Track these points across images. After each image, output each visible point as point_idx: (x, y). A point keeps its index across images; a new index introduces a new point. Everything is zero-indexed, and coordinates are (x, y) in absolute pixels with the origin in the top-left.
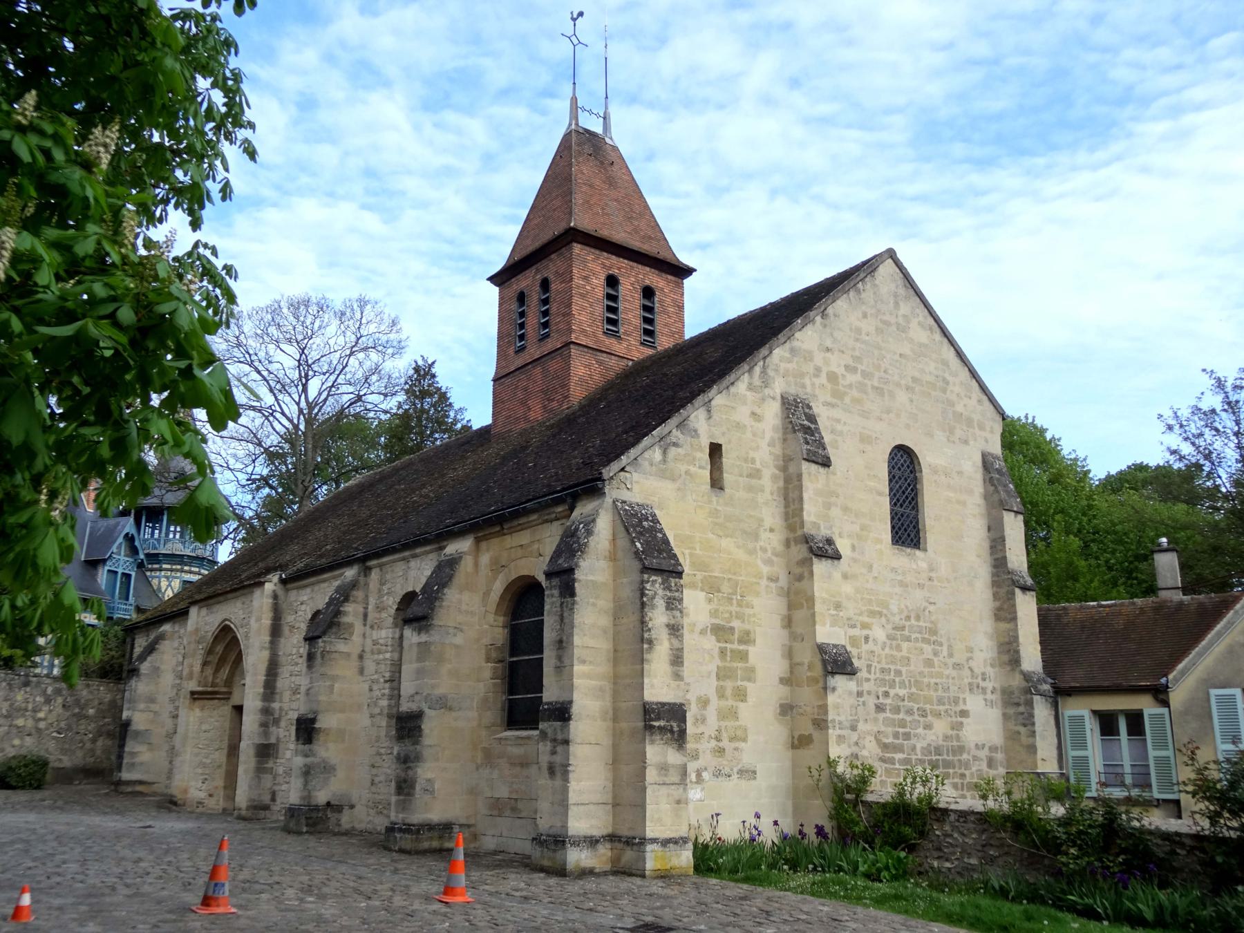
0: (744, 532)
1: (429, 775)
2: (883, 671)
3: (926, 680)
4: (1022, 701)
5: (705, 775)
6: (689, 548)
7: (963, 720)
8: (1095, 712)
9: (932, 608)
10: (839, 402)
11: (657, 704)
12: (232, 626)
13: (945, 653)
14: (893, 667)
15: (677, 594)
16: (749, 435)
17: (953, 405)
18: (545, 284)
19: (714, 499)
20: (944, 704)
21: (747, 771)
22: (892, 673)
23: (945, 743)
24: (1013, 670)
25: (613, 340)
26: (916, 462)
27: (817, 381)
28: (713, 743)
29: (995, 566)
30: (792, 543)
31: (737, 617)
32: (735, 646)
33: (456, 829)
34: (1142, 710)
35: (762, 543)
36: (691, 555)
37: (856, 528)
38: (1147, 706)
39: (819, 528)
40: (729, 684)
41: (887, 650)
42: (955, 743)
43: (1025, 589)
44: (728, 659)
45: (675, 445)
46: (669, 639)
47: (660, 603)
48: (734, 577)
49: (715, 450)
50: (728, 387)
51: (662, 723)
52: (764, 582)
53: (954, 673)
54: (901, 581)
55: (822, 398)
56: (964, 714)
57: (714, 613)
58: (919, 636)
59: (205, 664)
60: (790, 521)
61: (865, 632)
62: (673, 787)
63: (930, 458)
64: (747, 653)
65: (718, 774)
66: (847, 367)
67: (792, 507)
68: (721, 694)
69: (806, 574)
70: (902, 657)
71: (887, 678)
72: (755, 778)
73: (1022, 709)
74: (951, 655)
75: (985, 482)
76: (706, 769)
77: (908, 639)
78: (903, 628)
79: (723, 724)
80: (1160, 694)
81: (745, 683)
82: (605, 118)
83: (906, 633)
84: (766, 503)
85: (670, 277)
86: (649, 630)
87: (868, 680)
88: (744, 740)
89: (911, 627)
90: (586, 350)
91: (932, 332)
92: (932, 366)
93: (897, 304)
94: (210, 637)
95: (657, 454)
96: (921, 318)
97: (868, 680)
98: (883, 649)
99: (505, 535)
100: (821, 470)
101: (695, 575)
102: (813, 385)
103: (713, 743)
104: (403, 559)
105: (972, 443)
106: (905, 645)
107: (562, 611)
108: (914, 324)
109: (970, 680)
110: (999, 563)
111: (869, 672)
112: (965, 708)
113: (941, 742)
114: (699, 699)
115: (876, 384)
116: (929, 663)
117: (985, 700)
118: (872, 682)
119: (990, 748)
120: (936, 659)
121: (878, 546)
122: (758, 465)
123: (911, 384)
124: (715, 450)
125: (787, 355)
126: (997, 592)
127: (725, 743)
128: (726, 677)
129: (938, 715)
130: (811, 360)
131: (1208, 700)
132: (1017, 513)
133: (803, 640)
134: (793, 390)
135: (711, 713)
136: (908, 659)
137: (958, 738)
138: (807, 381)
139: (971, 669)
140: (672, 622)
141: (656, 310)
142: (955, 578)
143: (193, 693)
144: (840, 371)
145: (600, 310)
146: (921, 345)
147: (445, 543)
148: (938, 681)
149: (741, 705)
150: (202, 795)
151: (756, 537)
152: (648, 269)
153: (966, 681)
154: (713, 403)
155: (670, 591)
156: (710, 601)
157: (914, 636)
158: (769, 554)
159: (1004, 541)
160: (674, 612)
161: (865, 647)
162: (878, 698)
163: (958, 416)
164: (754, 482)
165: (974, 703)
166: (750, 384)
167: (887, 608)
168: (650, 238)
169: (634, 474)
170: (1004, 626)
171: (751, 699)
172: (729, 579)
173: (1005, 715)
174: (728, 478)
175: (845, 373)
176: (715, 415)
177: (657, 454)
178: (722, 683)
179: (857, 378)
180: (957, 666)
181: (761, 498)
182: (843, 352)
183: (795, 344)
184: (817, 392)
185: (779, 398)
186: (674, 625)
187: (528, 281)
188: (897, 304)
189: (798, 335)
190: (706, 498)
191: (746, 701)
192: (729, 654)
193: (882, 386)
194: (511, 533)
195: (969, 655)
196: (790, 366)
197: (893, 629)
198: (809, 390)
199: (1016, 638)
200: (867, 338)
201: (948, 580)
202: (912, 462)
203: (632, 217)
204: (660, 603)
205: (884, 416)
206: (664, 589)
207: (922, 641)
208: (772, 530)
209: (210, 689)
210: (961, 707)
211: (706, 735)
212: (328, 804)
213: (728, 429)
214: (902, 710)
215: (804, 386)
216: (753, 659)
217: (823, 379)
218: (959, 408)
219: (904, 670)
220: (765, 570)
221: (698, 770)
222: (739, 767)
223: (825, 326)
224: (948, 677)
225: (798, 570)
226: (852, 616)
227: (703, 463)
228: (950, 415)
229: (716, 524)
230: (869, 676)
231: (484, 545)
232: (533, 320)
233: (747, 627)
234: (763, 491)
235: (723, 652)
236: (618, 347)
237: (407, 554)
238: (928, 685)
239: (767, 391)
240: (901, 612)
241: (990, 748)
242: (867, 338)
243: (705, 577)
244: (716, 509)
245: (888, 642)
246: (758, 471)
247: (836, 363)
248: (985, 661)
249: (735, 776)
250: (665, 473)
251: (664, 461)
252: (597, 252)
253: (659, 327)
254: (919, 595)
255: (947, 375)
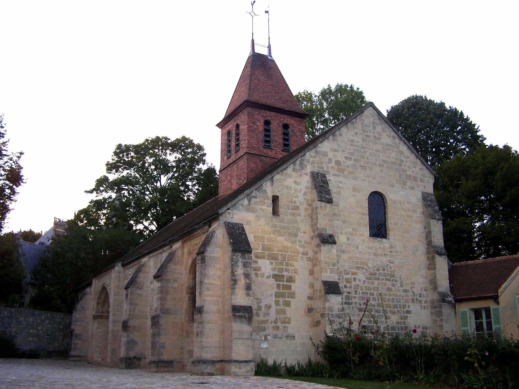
0: (290, 234)
1: (163, 341)
2: (363, 293)
3: (387, 297)
4: (437, 306)
5: (269, 337)
6: (261, 241)
7: (407, 315)
8: (472, 309)
9: (391, 265)
10: (341, 174)
11: (238, 306)
12: (106, 286)
13: (399, 285)
14: (369, 292)
15: (248, 261)
16: (293, 191)
17: (406, 171)
18: (238, 126)
19: (275, 220)
20: (397, 308)
21: (291, 336)
22: (369, 294)
23: (397, 325)
24: (434, 292)
25: (268, 151)
26: (385, 199)
27: (330, 165)
28: (273, 324)
29: (428, 245)
30: (314, 238)
31: (286, 271)
32: (285, 283)
33: (175, 363)
34: (490, 307)
35: (299, 238)
36: (262, 245)
37: (350, 230)
38: (492, 305)
39: (326, 230)
40: (281, 300)
41: (366, 284)
42: (403, 325)
43: (440, 254)
44: (281, 289)
45: (255, 197)
46: (245, 279)
47: (240, 264)
48: (284, 253)
49: (275, 199)
50: (282, 171)
51: (240, 314)
52: (300, 255)
53: (404, 294)
54: (375, 253)
55: (332, 172)
56: (408, 312)
57: (273, 269)
58: (384, 277)
59: (98, 303)
60: (314, 228)
61: (353, 276)
62: (245, 340)
63: (390, 196)
64: (291, 286)
65: (275, 337)
66: (346, 158)
67: (314, 222)
68: (277, 303)
69: (319, 251)
70: (374, 287)
71: (366, 296)
72: (294, 339)
73: (438, 309)
74: (402, 286)
75: (423, 206)
76: (269, 335)
77: (378, 279)
78: (375, 274)
79: (278, 316)
80: (496, 299)
81: (290, 299)
82: (269, 47)
83: (377, 276)
84: (302, 221)
85: (297, 119)
86: (235, 276)
87: (355, 297)
88: (289, 323)
89: (380, 274)
90: (254, 155)
91: (394, 139)
92: (394, 155)
93: (374, 128)
94: (99, 292)
95: (246, 202)
96: (388, 133)
97: (355, 297)
98: (364, 284)
99: (191, 240)
100: (328, 205)
101: (264, 253)
102: (328, 167)
103: (273, 324)
104: (161, 253)
105: (416, 188)
106: (376, 282)
107: (201, 269)
108: (384, 135)
109: (413, 297)
110: (429, 243)
111: (356, 294)
112: (409, 310)
113: (395, 325)
114: (266, 305)
115: (362, 164)
116: (389, 289)
117: (421, 306)
118: (357, 298)
119: (423, 328)
120: (393, 288)
121: (362, 238)
122: (298, 204)
123: (381, 163)
124: (275, 199)
125: (314, 154)
126: (428, 257)
127: (279, 324)
128: (279, 296)
129: (394, 313)
130: (327, 156)
131: (515, 300)
132: (438, 220)
133: (317, 280)
134: (316, 170)
135: (273, 311)
136: (378, 288)
137: (404, 323)
138: (324, 165)
139: (413, 292)
140: (246, 272)
141: (290, 134)
142: (405, 251)
143: (94, 316)
144: (342, 160)
145: (261, 137)
146: (387, 145)
147: (173, 245)
148: (394, 297)
149: (287, 308)
150: (100, 359)
151: (296, 235)
152: (286, 116)
153: (410, 297)
154: (274, 178)
155: (245, 259)
156: (272, 263)
157: (381, 278)
158: (303, 243)
159: (431, 233)
160: (247, 268)
161: (354, 283)
162: (360, 305)
163: (409, 177)
164: (295, 212)
165: (414, 308)
166: (294, 168)
167: (367, 265)
168: (288, 101)
169: (234, 211)
170: (430, 272)
171: (293, 306)
172: (282, 255)
173: (432, 313)
174: (281, 210)
175: (345, 161)
176: (276, 184)
177: (246, 202)
178: (277, 299)
179: (352, 162)
180: (405, 291)
181: (299, 219)
182: (344, 151)
183: (318, 149)
184: (330, 170)
185: (309, 173)
186: (247, 274)
187: (231, 126)
188: (374, 128)
189: (319, 145)
190: (270, 219)
191: (290, 307)
192: (281, 286)
193: (365, 165)
194: (193, 239)
195: (412, 286)
196: (315, 159)
197: (370, 275)
198: (325, 169)
199: (436, 277)
200: (357, 144)
201: (401, 252)
202: (383, 199)
203: (279, 92)
204: (240, 264)
205: (366, 179)
206: (242, 258)
207: (386, 280)
208: (304, 232)
209: (101, 314)
210: (407, 309)
211: (270, 321)
212: (135, 357)
213: (282, 189)
214: (373, 310)
215: (322, 168)
216: (293, 288)
217: (333, 164)
218: (409, 173)
219: (375, 293)
220: (301, 250)
221: (265, 335)
222: (286, 334)
223: (334, 140)
224: (400, 296)
225: (316, 249)
226: (347, 269)
227: (269, 204)
228: (404, 177)
229: (275, 231)
230: (356, 296)
231: (185, 245)
232: (233, 144)
233: (290, 274)
234: (300, 215)
235: (278, 286)
236: (271, 153)
237: (161, 250)
238: (389, 300)
239: (303, 171)
240: (374, 267)
241: (423, 328)
242: (357, 144)
243: (269, 253)
244: (275, 224)
245: (367, 281)
246: (297, 206)
247: (340, 157)
248: (421, 288)
249: (284, 339)
250: (248, 209)
251: (249, 204)
252: (260, 110)
253: (291, 142)
254: (385, 259)
255: (402, 158)
